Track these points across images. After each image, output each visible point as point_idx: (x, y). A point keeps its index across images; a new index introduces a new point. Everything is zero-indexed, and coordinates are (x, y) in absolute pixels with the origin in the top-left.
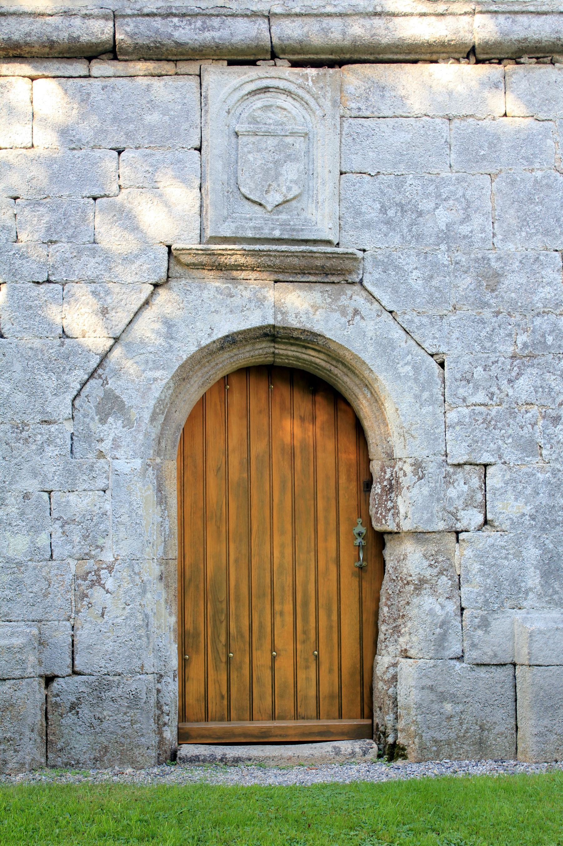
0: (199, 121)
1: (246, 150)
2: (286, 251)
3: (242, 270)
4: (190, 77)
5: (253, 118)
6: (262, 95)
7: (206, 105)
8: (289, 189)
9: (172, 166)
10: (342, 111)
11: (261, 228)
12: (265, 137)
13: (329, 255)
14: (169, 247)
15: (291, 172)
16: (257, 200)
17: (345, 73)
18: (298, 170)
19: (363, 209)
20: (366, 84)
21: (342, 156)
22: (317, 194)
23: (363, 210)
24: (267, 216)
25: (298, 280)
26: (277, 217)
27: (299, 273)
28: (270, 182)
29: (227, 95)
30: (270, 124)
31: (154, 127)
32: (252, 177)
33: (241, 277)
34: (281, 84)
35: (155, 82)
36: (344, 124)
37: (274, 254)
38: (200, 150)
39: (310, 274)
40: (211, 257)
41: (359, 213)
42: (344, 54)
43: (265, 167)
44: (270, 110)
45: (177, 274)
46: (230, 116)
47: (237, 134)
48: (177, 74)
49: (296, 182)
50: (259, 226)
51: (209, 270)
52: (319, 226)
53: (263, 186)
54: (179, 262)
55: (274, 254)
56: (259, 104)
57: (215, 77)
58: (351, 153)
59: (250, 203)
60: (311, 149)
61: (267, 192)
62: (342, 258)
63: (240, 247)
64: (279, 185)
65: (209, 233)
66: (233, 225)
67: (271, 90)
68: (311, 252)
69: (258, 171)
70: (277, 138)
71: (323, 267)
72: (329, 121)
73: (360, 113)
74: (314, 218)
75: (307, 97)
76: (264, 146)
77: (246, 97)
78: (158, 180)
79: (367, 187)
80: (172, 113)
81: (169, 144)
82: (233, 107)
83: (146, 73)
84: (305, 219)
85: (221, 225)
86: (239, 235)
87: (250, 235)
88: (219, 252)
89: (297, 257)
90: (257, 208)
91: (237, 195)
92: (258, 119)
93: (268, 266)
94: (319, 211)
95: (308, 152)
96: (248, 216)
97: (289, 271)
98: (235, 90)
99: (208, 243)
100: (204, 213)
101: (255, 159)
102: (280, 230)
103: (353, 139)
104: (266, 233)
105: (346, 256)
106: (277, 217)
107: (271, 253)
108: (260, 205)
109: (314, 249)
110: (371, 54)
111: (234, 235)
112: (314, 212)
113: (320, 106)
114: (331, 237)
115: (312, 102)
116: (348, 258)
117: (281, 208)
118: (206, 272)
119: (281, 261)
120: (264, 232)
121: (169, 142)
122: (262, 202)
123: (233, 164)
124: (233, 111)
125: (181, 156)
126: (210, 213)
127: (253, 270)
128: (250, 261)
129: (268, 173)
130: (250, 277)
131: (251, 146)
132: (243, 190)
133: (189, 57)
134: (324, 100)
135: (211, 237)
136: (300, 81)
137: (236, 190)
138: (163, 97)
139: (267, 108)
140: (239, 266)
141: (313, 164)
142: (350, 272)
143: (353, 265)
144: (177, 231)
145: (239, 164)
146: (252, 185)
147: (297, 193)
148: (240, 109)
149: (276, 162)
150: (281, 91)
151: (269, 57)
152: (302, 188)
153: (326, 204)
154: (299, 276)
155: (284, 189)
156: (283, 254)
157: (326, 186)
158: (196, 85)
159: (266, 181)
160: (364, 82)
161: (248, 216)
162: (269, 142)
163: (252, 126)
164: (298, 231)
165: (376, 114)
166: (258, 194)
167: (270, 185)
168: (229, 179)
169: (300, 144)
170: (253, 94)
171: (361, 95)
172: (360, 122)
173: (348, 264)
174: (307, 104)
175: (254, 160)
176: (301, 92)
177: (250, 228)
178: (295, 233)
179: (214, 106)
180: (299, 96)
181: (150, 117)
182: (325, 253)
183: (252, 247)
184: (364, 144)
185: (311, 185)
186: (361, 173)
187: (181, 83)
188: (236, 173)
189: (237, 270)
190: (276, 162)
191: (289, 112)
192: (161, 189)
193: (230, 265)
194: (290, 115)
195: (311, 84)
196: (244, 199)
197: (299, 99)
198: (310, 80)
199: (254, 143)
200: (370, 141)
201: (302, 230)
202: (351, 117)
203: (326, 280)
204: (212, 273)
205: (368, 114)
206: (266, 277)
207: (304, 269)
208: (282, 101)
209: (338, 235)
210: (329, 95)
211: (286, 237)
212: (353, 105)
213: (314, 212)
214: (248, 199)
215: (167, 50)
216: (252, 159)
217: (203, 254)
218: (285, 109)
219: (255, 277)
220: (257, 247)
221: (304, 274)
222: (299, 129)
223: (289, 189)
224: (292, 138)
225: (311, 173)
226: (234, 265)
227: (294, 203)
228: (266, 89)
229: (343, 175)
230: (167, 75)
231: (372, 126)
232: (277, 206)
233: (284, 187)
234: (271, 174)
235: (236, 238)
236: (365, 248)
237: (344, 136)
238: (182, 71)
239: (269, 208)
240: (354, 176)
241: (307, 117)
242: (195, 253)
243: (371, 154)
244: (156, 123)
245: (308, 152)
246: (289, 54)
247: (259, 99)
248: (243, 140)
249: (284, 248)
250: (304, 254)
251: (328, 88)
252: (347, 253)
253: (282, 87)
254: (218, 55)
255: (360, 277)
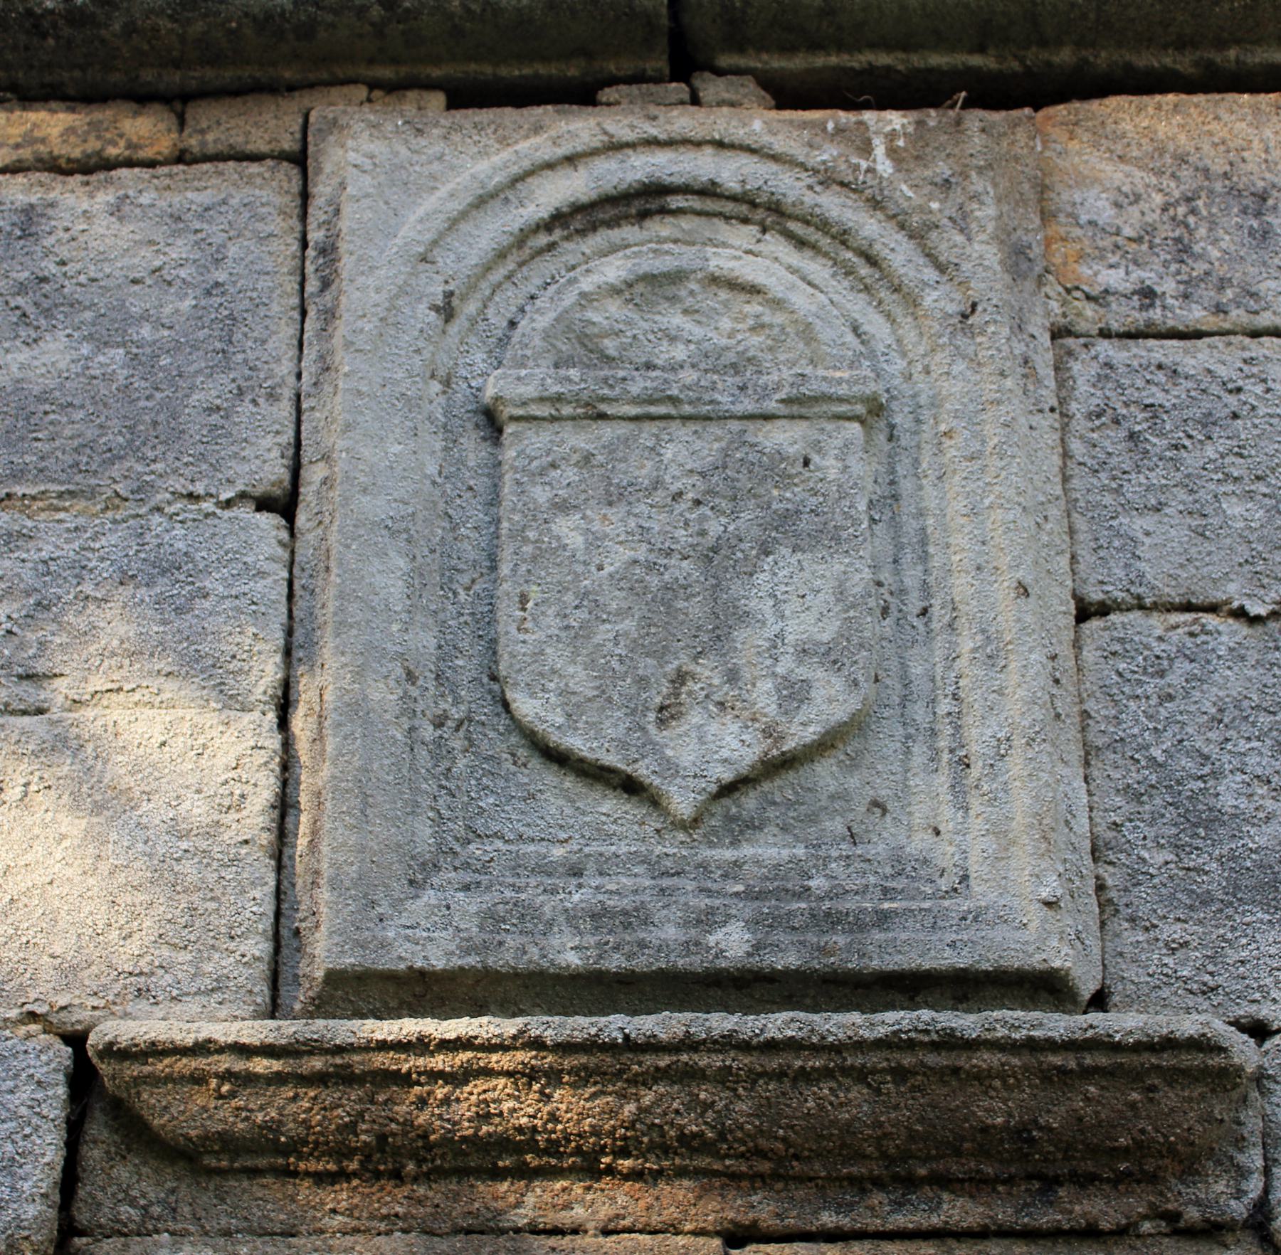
0: (285, 368)
1: (541, 495)
2: (792, 1045)
3: (525, 1174)
4: (254, 168)
5: (584, 339)
6: (629, 232)
7: (326, 284)
8: (794, 693)
9: (127, 591)
10: (1054, 305)
11: (635, 917)
12: (653, 427)
13: (1056, 1060)
14: (76, 1040)
15: (797, 601)
16: (611, 759)
17: (1058, 133)
18: (840, 592)
19: (1228, 796)
20: (1167, 182)
21: (1081, 523)
22: (955, 719)
23: (1228, 801)
24: (671, 847)
25: (875, 1224)
26: (729, 854)
27: (879, 1183)
28: (682, 660)
29: (439, 223)
30: (675, 367)
31: (39, 399)
32: (577, 637)
33: (521, 1217)
34: (730, 172)
35: (72, 199)
36: (1076, 367)
37: (717, 1061)
38: (284, 504)
39: (943, 1181)
40: (329, 1095)
41: (1201, 820)
42: (1044, 43)
43: (654, 581)
44: (673, 299)
45: (126, 1211)
46: (453, 328)
47: (491, 422)
48: (182, 157)
49: (830, 656)
50: (626, 903)
51: (321, 1179)
52: (982, 893)
53: (643, 683)
54: (138, 1135)
55: (717, 1061)
56: (614, 270)
57: (378, 147)
58: (1128, 507)
59: (569, 782)
60: (906, 486)
61: (667, 714)
62: (1136, 1077)
63: (509, 1027)
64: (732, 676)
65: (324, 952)
66: (470, 906)
67: (676, 202)
68: (950, 1042)
69: (614, 600)
70: (714, 429)
71: (1021, 1134)
72: (996, 338)
73: (1156, 314)
74: (945, 853)
75: (869, 227)
76: (644, 472)
77: (543, 239)
78: (41, 667)
79: (1232, 681)
80: (146, 331)
81: (117, 479)
82: (472, 287)
83: (26, 154)
84: (898, 859)
85: (397, 904)
86: (503, 959)
87: (573, 960)
88: (381, 1060)
89: (861, 1075)
90: (610, 805)
91: (496, 742)
92: (610, 346)
93: (683, 1138)
94: (976, 805)
95: (889, 499)
96: (558, 852)
97: (819, 1168)
98: (481, 202)
99: (321, 1007)
100: (302, 843)
101: (595, 541)
102: (753, 923)
103: (1132, 436)
104: (666, 940)
105: (1167, 1060)
106: (729, 854)
107: (703, 1060)
108: (631, 787)
109: (967, 1023)
110: (1181, 44)
111: (472, 961)
112: (948, 817)
113: (941, 268)
114: (1059, 956)
115: (900, 254)
116: (1174, 1076)
117: (750, 802)
118: (305, 1191)
119: (764, 1108)
120: (653, 936)
121: (116, 470)
122: (643, 770)
123: (469, 575)
124: (471, 308)
125: (179, 538)
126: (325, 840)
127: (590, 1169)
128: (574, 1109)
129: (670, 610)
130: (579, 1212)
131: (571, 474)
132: (526, 706)
133: (247, 73)
134: (959, 238)
135: (334, 978)
136: (827, 154)
137: (485, 711)
138: (102, 258)
139: (656, 286)
140: (503, 1144)
141: (925, 558)
142: (1190, 1161)
143: (1208, 1118)
144: (134, 947)
145: (505, 570)
146: (580, 679)
147: (840, 713)
148: (510, 298)
149: (709, 555)
150: (729, 207)
151: (659, 63)
152: (867, 687)
153: (1016, 765)
154: (877, 1198)
155: (764, 697)
156: (774, 1063)
157: (1003, 672)
158: (278, 200)
159: (661, 654)
160: (1159, 173)
161: (558, 852)
162: (669, 453)
163: (574, 373)
164: (857, 925)
165: (1238, 316)
166: (615, 725)
167: (681, 678)
168: (447, 652)
169: (842, 458)
170: (577, 223)
171: (1150, 230)
172: (1158, 356)
173: (1181, 1112)
174: (872, 261)
175: (590, 535)
176: (833, 205)
177: (571, 918)
178: (841, 940)
179: (364, 289)
180: (824, 225)
181: (24, 355)
182: (1032, 1045)
183: (580, 1026)
184: (1191, 461)
185: (916, 670)
186: (1188, 607)
187: (205, 198)
188: (486, 620)
189: (497, 1174)
190: (709, 555)
191: (778, 304)
192: (56, 713)
193: (447, 1141)
194: (779, 318)
195: (885, 167)
196: (536, 763)
197: (825, 242)
198: (880, 150)
199: (588, 458)
200: (1222, 445)
201: (883, 919)
202: (1105, 334)
203: (1047, 1218)
204: (341, 1196)
205: (1196, 315)
206: (671, 1213)
207: (905, 1156)
208: (738, 251)
209: (1093, 942)
210: (986, 212)
211: (789, 959)
212: (1113, 278)
213: (948, 817)
214: (558, 758)
215: (130, 29)
216: (576, 541)
217: (279, 1079)
218: (754, 290)
219: (605, 1211)
220: (615, 1025)
221: (910, 1183)
222: (838, 378)
223: (794, 693)
224: (800, 428)
225: (914, 605)
226: (473, 1141)
227: (825, 773)
228: (647, 201)
229: (1095, 624)
230: (130, 163)
231: (1222, 371)
232: (727, 790)
233: (766, 685)
234: (692, 615)
235: (488, 977)
236: (1265, 1012)
237: (1080, 424)
238: (214, 139)
239: (682, 803)
240: (1157, 623)
241: (876, 325)
242: (228, 1076)
243: (1234, 508)
244: (51, 383)
245: (889, 499)
246: (762, 46)
247: (613, 249)
248: (523, 445)
249: (778, 1024)
250: (907, 1060)
251: (978, 183)
252: (1169, 1043)
253: (733, 186)
254: (395, 61)
255: (1254, 1186)
